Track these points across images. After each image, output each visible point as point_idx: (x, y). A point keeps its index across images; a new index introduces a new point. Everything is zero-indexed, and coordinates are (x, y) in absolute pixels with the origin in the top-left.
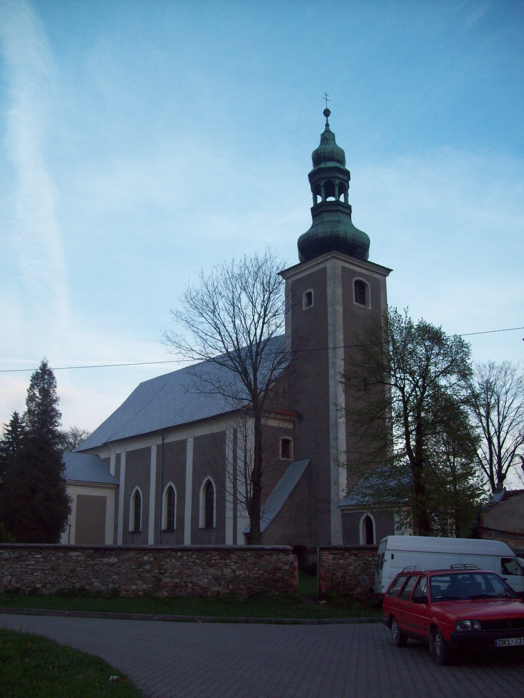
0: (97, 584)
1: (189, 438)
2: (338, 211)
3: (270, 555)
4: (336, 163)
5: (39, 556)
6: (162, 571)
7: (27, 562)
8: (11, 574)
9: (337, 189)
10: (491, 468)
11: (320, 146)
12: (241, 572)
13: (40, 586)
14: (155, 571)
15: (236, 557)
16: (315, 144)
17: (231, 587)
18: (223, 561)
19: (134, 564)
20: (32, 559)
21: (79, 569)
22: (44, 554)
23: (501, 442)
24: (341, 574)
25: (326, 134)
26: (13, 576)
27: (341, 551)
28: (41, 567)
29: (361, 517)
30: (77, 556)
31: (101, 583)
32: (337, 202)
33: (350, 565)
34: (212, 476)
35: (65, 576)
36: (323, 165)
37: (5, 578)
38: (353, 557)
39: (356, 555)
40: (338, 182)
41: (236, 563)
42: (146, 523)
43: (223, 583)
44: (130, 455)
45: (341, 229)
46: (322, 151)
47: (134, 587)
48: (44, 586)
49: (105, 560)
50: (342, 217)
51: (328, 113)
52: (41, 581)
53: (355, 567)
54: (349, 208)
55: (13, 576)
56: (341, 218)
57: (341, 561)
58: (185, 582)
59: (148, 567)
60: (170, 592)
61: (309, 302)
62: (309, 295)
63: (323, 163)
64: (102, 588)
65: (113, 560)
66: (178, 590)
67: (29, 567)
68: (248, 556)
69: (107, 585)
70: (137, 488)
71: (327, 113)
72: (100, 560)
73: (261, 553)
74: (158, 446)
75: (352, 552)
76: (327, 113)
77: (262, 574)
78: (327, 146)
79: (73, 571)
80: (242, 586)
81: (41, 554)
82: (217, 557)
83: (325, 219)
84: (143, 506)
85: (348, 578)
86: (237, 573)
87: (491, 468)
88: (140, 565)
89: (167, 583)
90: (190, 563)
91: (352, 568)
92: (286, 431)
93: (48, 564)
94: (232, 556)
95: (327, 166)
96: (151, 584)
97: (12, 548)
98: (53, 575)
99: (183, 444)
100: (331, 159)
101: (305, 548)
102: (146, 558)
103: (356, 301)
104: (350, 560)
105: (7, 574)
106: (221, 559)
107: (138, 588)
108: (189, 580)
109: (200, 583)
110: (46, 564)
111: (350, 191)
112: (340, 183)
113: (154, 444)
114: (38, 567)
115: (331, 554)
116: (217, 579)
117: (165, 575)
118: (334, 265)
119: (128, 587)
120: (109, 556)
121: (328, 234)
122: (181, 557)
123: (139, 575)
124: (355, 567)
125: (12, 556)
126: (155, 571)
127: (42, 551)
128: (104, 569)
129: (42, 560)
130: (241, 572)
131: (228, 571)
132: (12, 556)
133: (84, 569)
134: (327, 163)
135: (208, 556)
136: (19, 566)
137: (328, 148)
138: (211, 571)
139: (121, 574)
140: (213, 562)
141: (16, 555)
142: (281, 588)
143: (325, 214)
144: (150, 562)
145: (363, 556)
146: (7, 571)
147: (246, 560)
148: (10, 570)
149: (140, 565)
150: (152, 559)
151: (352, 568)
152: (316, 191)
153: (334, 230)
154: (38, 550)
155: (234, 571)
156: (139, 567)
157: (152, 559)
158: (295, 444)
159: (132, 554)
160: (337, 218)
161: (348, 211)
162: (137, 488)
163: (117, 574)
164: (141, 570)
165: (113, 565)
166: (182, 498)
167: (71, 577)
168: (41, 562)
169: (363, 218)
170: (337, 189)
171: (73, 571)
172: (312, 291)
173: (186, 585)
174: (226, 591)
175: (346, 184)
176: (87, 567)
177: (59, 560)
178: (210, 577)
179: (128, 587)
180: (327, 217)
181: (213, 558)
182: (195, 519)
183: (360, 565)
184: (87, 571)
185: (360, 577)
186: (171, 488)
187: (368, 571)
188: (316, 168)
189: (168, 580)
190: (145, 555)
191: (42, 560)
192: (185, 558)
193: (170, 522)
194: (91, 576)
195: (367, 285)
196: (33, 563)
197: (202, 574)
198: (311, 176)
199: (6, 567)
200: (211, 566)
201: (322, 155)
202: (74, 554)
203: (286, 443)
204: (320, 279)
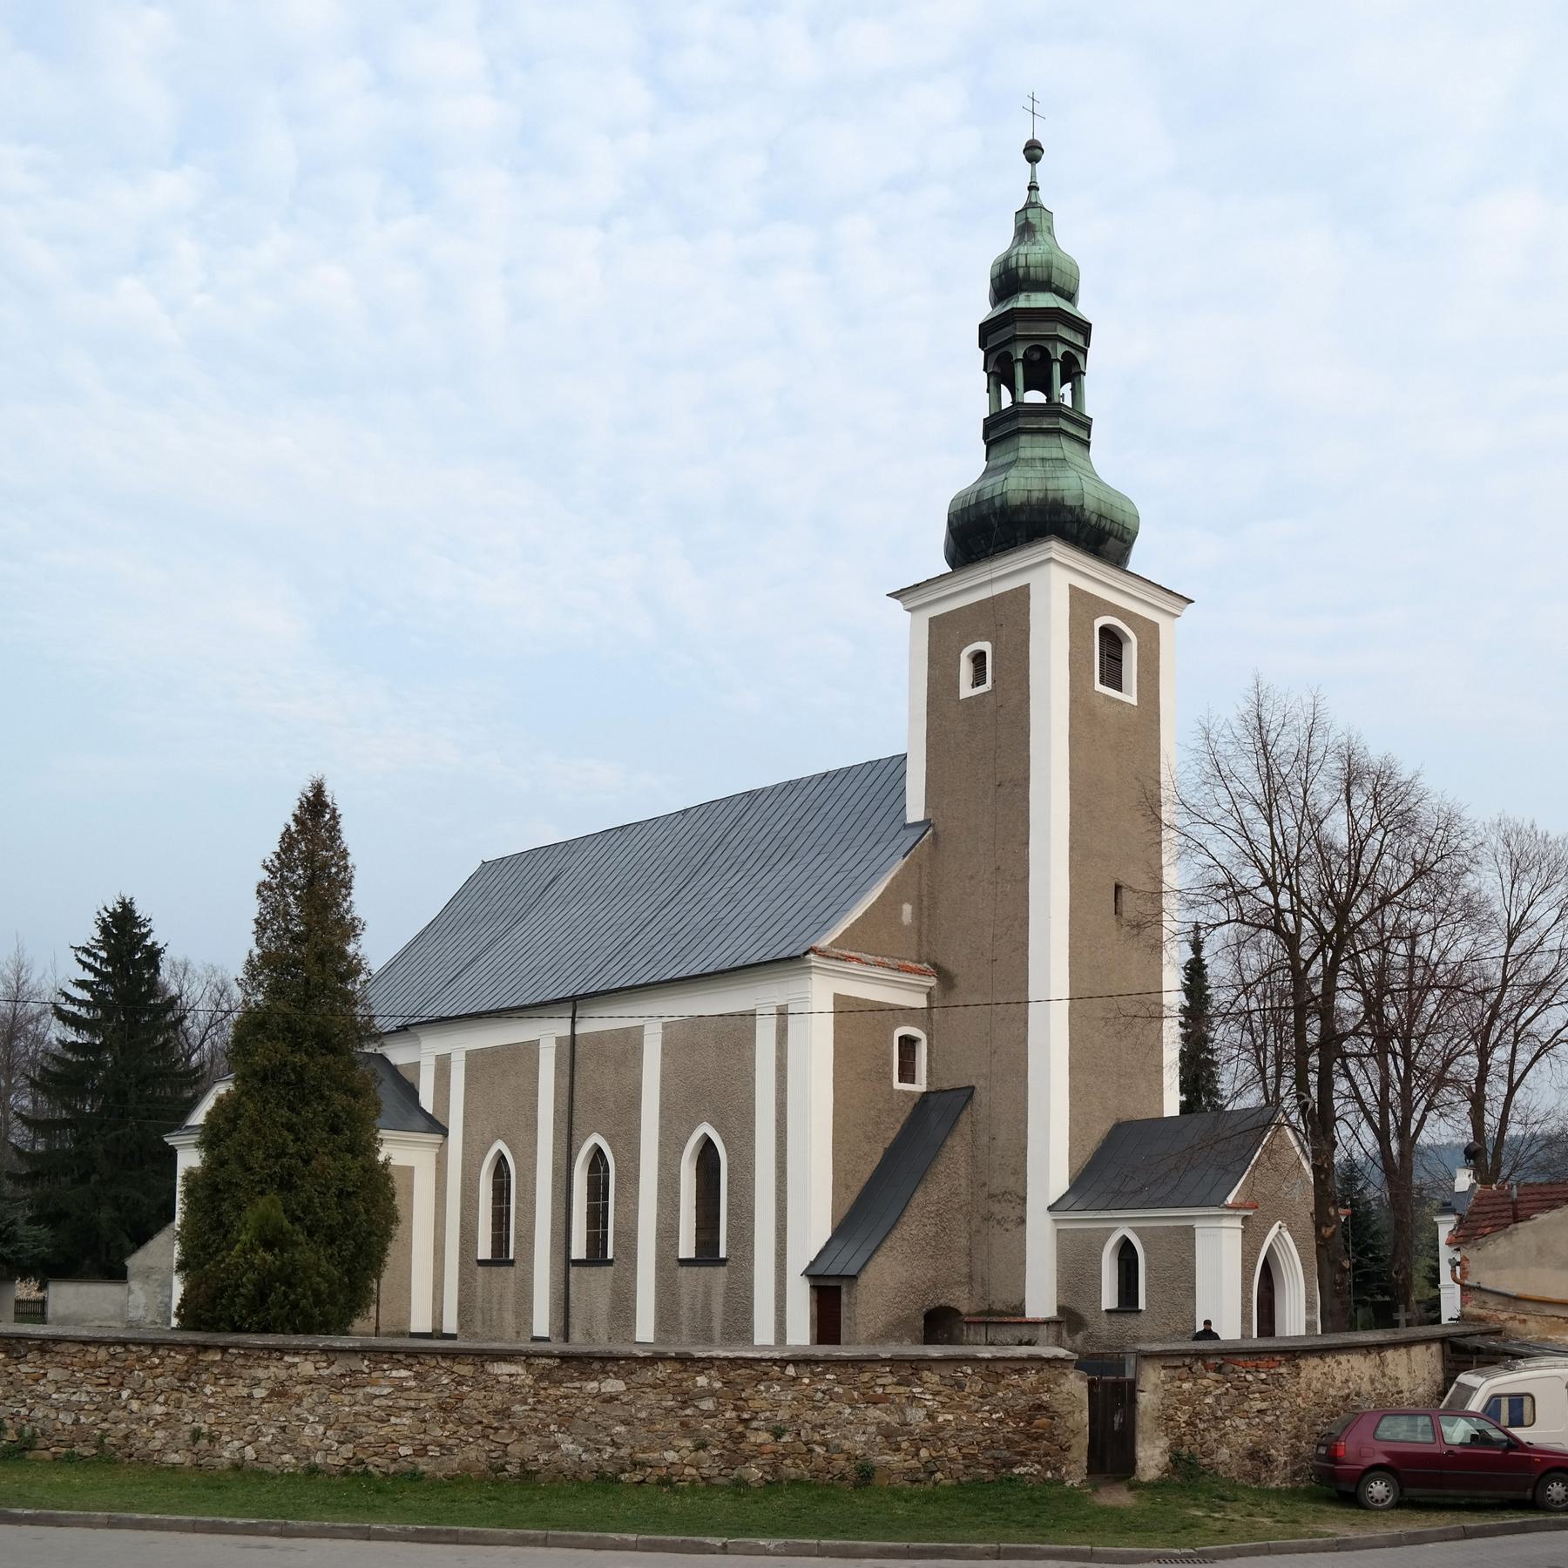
0: (568, 1446)
1: (652, 1021)
2: (1060, 432)
3: (1020, 1372)
4: (1058, 299)
5: (404, 1373)
6: (746, 1416)
7: (368, 1390)
8: (323, 1419)
9: (1057, 369)
10: (1384, 1117)
11: (1012, 247)
12: (950, 1417)
13: (410, 1452)
14: (728, 1415)
15: (937, 1378)
16: (999, 240)
17: (924, 1453)
18: (902, 1389)
19: (670, 1397)
20: (383, 1382)
21: (517, 1408)
22: (417, 1368)
23: (1516, 1077)
24: (1185, 1418)
25: (1030, 213)
26: (329, 1427)
27: (1187, 1361)
28: (412, 1404)
29: (1108, 1238)
30: (511, 1375)
31: (581, 1444)
32: (1052, 409)
33: (1205, 1394)
34: (716, 1127)
35: (479, 1428)
36: (1022, 302)
37: (307, 1431)
38: (1211, 1375)
39: (1218, 1369)
40: (1061, 349)
41: (937, 1393)
42: (527, 1239)
43: (904, 1445)
44: (476, 1061)
45: (1067, 485)
46: (1022, 262)
47: (671, 1456)
48: (422, 1451)
49: (592, 1386)
50: (1069, 449)
51: (1038, 152)
52: (413, 1438)
53: (1218, 1398)
54: (1086, 425)
55: (329, 1427)
56: (1068, 454)
57: (1186, 1386)
58: (806, 1444)
59: (707, 1405)
60: (767, 1468)
61: (979, 679)
62: (979, 658)
63: (1022, 296)
64: (584, 1457)
65: (613, 1385)
66: (788, 1462)
67: (376, 1402)
68: (966, 1375)
69: (599, 1450)
70: (500, 1145)
71: (1033, 152)
72: (577, 1384)
73: (1000, 1368)
74: (559, 1040)
75: (1211, 1361)
76: (1033, 152)
77: (1000, 1421)
78: (1036, 249)
79: (504, 1413)
80: (953, 1451)
81: (408, 1367)
82: (889, 1379)
83: (1025, 453)
84: (518, 1192)
85: (1201, 1426)
86: (940, 1419)
87: (1384, 1117)
88: (687, 1399)
89: (761, 1445)
90: (820, 1395)
91: (1209, 1400)
92: (906, 1014)
93: (431, 1396)
94: (926, 1374)
95: (1033, 305)
96: (715, 1447)
97: (325, 1351)
98: (445, 1423)
99: (630, 1043)
100: (1045, 285)
101: (956, 1312)
102: (702, 1381)
103: (1102, 682)
104: (1205, 1382)
105: (311, 1419)
106: (898, 1384)
107: (682, 1458)
108: (817, 1437)
109: (847, 1445)
110: (425, 1395)
111: (1088, 381)
112: (1066, 354)
113: (548, 1034)
114: (402, 1403)
115: (1164, 1367)
116: (889, 1435)
117: (755, 1424)
118: (1053, 579)
119: (656, 1455)
120: (601, 1377)
121: (1035, 495)
122: (794, 1379)
123: (682, 1424)
124: (1218, 1398)
125: (327, 1372)
126: (728, 1415)
127: (411, 1361)
128: (588, 1410)
129: (412, 1383)
130: (950, 1417)
131: (916, 1415)
132: (325, 1372)
133: (534, 1410)
134: (1033, 296)
135: (866, 1377)
136: (347, 1399)
137: (1033, 253)
138: (874, 1413)
139: (637, 1423)
140: (880, 1390)
141: (336, 1369)
142: (1047, 1455)
143: (1024, 440)
144: (710, 1393)
145: (1233, 1371)
146: (311, 1411)
147: (962, 1388)
148: (320, 1410)
149: (687, 1399)
150: (717, 1385)
151: (1209, 1400)
152: (999, 371)
153: (1051, 485)
154: (401, 1357)
155: (931, 1416)
156: (684, 1404)
157: (717, 1385)
158: (929, 1044)
159: (663, 1371)
160: (1056, 453)
161: (1083, 435)
162: (500, 1145)
163: (624, 1423)
164: (688, 1412)
165: (611, 1399)
166: (630, 1177)
167: (497, 1429)
168: (410, 1389)
169: (1119, 458)
170: (1057, 369)
171: (504, 1413)
172: (986, 646)
173: (811, 1451)
174: (914, 1463)
175: (1080, 358)
176: (539, 1402)
177: (459, 1383)
178: (872, 1429)
179: (656, 1455)
180: (1030, 448)
181: (879, 1381)
182: (667, 1233)
183: (1227, 1392)
184: (541, 1415)
185: (1228, 1422)
186: (598, 1152)
187: (1246, 1406)
188: (1001, 309)
189: (764, 1437)
190: (700, 1373)
191: (412, 1383)
192: (806, 1381)
193: (596, 1241)
194: (553, 1427)
195: (1128, 639)
196: (385, 1391)
197: (851, 1423)
198: (987, 331)
199: (307, 1402)
200: (874, 1402)
201: (1021, 272)
202: (502, 1369)
203: (908, 1043)
204: (1007, 620)
